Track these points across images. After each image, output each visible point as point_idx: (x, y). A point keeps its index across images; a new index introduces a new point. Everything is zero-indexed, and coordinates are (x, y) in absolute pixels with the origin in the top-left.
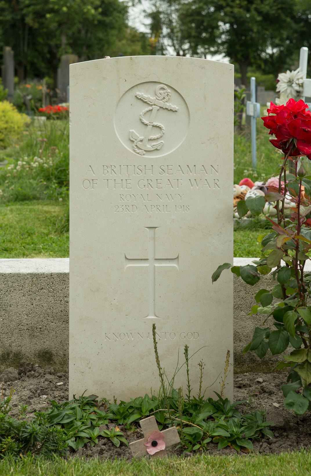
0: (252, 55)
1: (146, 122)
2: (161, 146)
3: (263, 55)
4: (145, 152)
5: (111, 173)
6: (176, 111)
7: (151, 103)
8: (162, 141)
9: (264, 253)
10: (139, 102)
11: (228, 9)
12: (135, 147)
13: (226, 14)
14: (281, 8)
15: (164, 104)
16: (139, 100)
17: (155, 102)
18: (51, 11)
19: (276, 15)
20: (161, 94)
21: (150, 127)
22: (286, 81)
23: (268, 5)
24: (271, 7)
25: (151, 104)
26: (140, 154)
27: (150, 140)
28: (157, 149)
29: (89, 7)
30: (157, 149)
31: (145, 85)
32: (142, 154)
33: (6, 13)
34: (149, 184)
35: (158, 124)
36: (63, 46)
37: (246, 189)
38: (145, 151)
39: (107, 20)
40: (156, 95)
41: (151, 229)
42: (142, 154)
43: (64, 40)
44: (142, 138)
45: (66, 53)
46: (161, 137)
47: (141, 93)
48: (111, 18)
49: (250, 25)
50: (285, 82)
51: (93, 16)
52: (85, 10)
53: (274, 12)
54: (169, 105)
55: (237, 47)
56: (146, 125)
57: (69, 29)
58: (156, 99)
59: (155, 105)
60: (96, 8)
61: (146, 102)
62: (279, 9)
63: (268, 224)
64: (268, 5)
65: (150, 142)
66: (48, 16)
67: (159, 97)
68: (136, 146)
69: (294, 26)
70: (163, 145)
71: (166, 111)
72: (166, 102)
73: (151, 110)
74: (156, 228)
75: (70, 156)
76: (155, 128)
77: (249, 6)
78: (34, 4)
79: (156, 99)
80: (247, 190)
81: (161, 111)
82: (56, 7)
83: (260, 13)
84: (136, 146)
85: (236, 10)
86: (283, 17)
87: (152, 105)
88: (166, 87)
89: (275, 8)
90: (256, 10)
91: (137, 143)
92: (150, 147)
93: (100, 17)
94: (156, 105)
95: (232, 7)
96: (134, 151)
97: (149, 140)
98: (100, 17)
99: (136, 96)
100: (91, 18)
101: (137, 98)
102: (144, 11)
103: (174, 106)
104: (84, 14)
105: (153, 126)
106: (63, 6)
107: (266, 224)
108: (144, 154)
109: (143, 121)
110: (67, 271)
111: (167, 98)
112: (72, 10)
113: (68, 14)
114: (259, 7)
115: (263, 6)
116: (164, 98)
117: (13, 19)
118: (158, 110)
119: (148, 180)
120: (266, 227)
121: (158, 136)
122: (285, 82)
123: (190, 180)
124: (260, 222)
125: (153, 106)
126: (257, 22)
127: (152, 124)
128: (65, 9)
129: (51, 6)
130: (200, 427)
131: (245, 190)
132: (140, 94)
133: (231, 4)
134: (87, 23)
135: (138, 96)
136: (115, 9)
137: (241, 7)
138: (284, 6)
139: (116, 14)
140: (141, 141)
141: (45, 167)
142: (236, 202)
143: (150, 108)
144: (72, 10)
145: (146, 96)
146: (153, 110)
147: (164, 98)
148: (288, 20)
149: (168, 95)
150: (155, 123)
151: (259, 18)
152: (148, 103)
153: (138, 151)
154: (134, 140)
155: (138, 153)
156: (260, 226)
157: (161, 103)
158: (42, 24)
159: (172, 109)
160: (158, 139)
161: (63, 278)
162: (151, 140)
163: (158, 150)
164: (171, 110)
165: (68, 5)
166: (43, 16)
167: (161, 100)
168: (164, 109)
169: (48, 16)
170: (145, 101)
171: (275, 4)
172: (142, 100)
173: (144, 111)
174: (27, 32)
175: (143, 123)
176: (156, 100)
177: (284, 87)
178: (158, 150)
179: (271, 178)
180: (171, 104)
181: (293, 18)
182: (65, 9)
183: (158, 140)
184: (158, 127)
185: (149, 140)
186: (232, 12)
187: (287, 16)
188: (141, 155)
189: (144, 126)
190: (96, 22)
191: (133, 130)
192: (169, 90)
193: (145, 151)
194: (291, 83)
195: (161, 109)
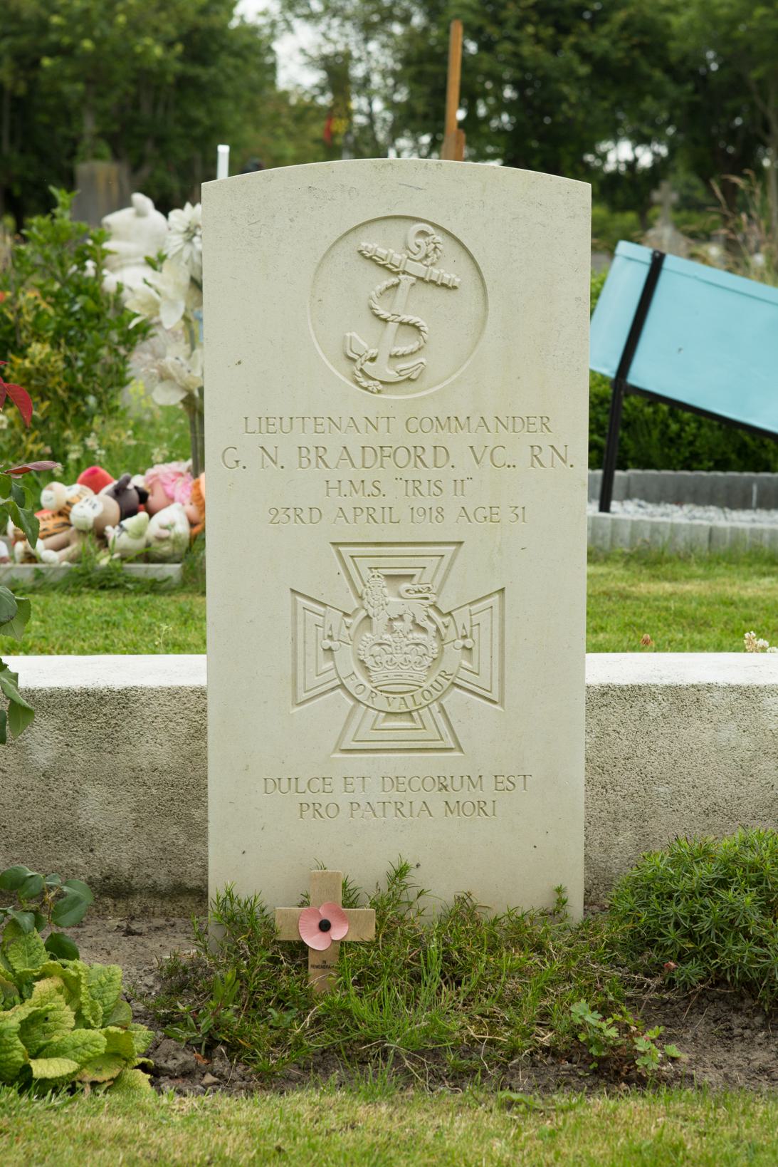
1: (385, 314)
2: (419, 371)
3: (663, 151)
4: (381, 387)
6: (455, 288)
7: (397, 267)
8: (423, 360)
9: (706, 602)
10: (368, 264)
12: (359, 374)
14: (641, 46)
15: (427, 271)
16: (368, 263)
17: (405, 266)
19: (627, 63)
20: (419, 246)
21: (393, 326)
22: (183, 229)
23: (606, 36)
24: (614, 43)
25: (396, 270)
26: (370, 391)
27: (395, 357)
29: (148, 41)
30: (409, 379)
31: (377, 225)
32: (375, 390)
34: (535, 456)
35: (414, 319)
36: (87, 141)
37: (81, 492)
38: (382, 382)
39: (203, 73)
40: (408, 248)
42: (375, 390)
43: (89, 126)
44: (373, 352)
45: (97, 156)
46: (419, 349)
47: (372, 243)
48: (213, 70)
50: (179, 232)
51: (160, 62)
52: (139, 49)
53: (620, 55)
54: (435, 273)
56: (385, 321)
58: (408, 258)
59: (404, 272)
60: (169, 45)
62: (633, 47)
63: (109, 576)
64: (606, 36)
65: (396, 360)
66: (46, 62)
67: (415, 254)
68: (361, 370)
69: (672, 90)
70: (423, 369)
71: (430, 287)
72: (432, 264)
73: (397, 286)
77: (560, 38)
79: (408, 258)
80: (81, 496)
81: (420, 285)
82: (66, 40)
83: (585, 56)
84: (361, 370)
85: (527, 50)
86: (644, 67)
87: (398, 273)
88: (430, 230)
89: (623, 44)
90: (577, 48)
91: (362, 365)
92: (395, 373)
93: (178, 67)
94: (409, 274)
95: (516, 42)
96: (357, 383)
97: (391, 356)
99: (360, 252)
100: (154, 66)
101: (363, 255)
102: (303, 51)
103: (448, 276)
104: (136, 57)
105: (401, 323)
106: (83, 36)
107: (103, 576)
108: (379, 392)
109: (376, 312)
110: (590, 656)
111: (433, 257)
112: (107, 48)
114: (584, 42)
115: (593, 38)
116: (427, 256)
118: (413, 285)
119: (532, 447)
120: (103, 584)
121: (413, 347)
122: (179, 232)
123: (471, 447)
124: (88, 573)
125: (402, 276)
126: (578, 79)
127: (399, 319)
128: (87, 44)
129: (53, 37)
131: (78, 496)
132: (370, 246)
135: (364, 252)
136: (223, 47)
137: (538, 40)
138: (647, 40)
139: (227, 61)
140: (373, 359)
142: (55, 524)
143: (394, 280)
144: (107, 48)
145: (382, 252)
146: (401, 285)
147: (427, 256)
148: (658, 74)
149: (436, 247)
150: (406, 318)
151: (584, 70)
153: (365, 384)
154: (356, 357)
155: (366, 389)
156: (87, 583)
157: (418, 269)
158: (32, 84)
159: (445, 282)
160: (412, 353)
162: (396, 356)
164: (443, 285)
165: (97, 33)
166: (36, 64)
167: (420, 261)
168: (426, 282)
170: (382, 263)
171: (625, 34)
172: (375, 261)
175: (377, 316)
176: (408, 261)
177: (175, 243)
179: (156, 466)
180: (442, 271)
181: (669, 70)
184: (413, 325)
185: (391, 356)
187: (653, 66)
188: (372, 392)
191: (354, 334)
192: (439, 238)
193: (382, 382)
194: (191, 234)
195: (419, 283)
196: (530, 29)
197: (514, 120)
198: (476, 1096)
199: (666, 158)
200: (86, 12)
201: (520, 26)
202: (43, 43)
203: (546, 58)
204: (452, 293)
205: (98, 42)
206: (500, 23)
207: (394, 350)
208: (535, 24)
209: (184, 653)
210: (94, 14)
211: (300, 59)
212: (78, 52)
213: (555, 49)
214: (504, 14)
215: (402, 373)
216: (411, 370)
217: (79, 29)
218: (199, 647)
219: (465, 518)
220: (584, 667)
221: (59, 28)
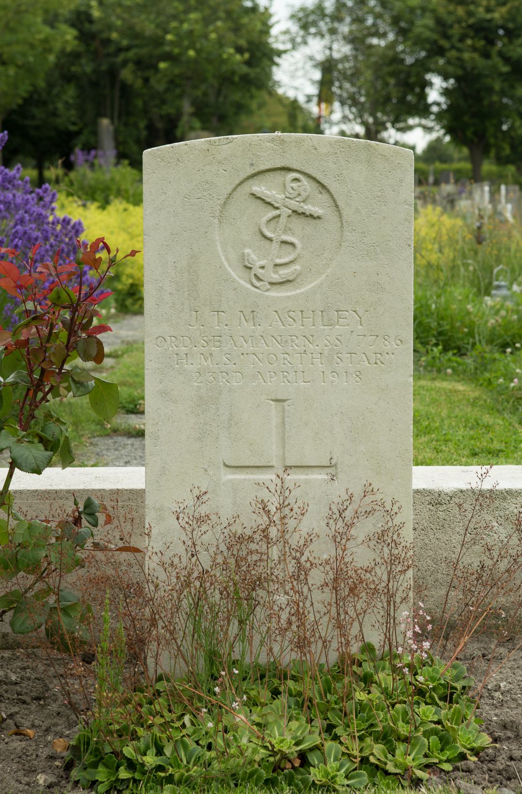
0: (491, 130)
5: (240, 323)
6: (319, 218)
11: (453, 53)
13: (449, 62)
16: (259, 201)
18: (168, 57)
31: (271, 174)
33: (83, 61)
36: (185, 118)
43: (187, 108)
48: (258, 70)
49: (489, 81)
52: (225, 56)
54: (308, 208)
55: (466, 118)
56: (270, 240)
57: (195, 87)
61: (269, 204)
66: (162, 65)
73: (279, 216)
78: (136, 46)
82: (176, 51)
83: (507, 60)
85: (466, 56)
90: (501, 54)
93: (245, 69)
95: (459, 50)
98: (245, 69)
102: (311, 58)
103: (317, 210)
104: (224, 62)
108: (267, 290)
112: (204, 55)
113: (196, 61)
115: (511, 47)
118: (289, 216)
126: (501, 74)
128: (191, 53)
129: (167, 48)
130: (331, 752)
133: (459, 45)
134: (227, 80)
137: (474, 49)
143: (277, 212)
146: (281, 217)
151: (505, 69)
157: (294, 205)
160: (292, 262)
161: (138, 495)
164: (303, 214)
165: (198, 46)
169: (162, 65)
172: (263, 200)
173: (265, 219)
174: (117, 93)
182: (191, 53)
186: (459, 59)
190: (236, 79)
196: (469, 42)
197: (449, 102)
198: (464, 768)
201: (461, 40)
202: (158, 52)
203: (480, 61)
204: (317, 221)
205: (198, 52)
206: (447, 37)
207: (278, 261)
208: (472, 38)
209: (507, 463)
211: (310, 64)
212: (184, 59)
213: (487, 55)
214: (451, 32)
218: (141, 461)
220: (411, 478)
221: (172, 43)
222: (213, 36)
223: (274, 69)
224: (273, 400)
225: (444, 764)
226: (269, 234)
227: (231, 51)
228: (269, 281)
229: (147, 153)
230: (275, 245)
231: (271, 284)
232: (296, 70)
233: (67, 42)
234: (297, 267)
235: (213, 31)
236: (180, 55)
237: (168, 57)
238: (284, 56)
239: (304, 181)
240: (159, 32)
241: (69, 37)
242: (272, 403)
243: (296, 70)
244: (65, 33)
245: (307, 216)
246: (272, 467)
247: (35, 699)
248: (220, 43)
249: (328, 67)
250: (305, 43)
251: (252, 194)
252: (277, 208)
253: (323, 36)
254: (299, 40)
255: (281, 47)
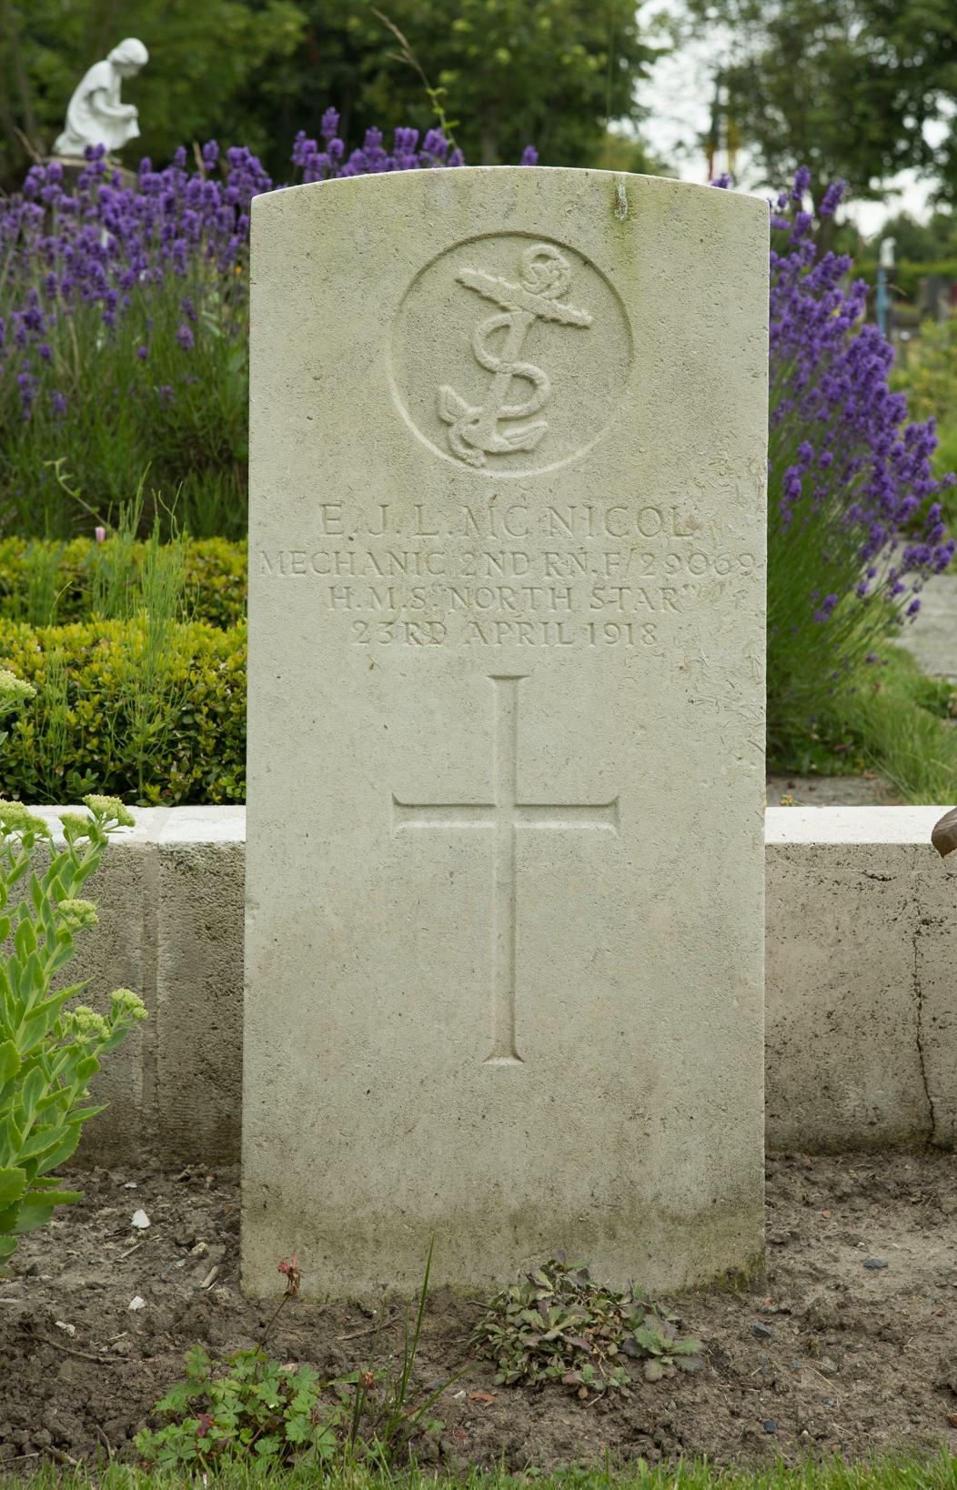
4: (483, 460)
6: (586, 328)
10: (469, 295)
12: (457, 442)
18: (457, 62)
27: (505, 420)
28: (523, 451)
41: (501, 682)
47: (471, 270)
52: (567, 60)
74: (519, 677)
75: (250, 458)
76: (518, 380)
82: (473, 50)
106: (496, 46)
112: (525, 59)
113: (509, 70)
117: (306, 89)
128: (503, 55)
129: (457, 47)
141: (829, 669)
146: (513, 330)
152: (495, 302)
159: (573, 320)
161: (236, 852)
163: (531, 452)
164: (554, 321)
165: (513, 41)
178: (531, 452)
182: (503, 55)
183: (534, 418)
189: (479, 375)
199: (949, 162)
200: (501, 16)
202: (440, 50)
204: (582, 334)
205: (514, 52)
210: (512, 17)
212: (488, 65)
215: (512, 440)
216: (521, 438)
217: (493, 35)
219: (480, 638)
221: (464, 36)
222: (545, 23)
223: (640, 83)
224: (495, 677)
225: (695, 1350)
226: (491, 360)
227: (579, 50)
228: (485, 448)
229: (258, 200)
230: (502, 382)
231: (487, 453)
232: (683, 85)
233: (287, 35)
234: (541, 423)
235: (544, 14)
236: (479, 59)
237: (457, 62)
238: (662, 61)
239: (564, 261)
240: (442, 17)
241: (291, 27)
242: (493, 683)
243: (683, 85)
244: (284, 19)
245: (547, 322)
246: (491, 806)
247: (261, 1309)
248: (557, 38)
249: (731, 79)
250: (695, 36)
251: (459, 281)
252: (504, 309)
253: (732, 24)
254: (686, 30)
255: (653, 43)
